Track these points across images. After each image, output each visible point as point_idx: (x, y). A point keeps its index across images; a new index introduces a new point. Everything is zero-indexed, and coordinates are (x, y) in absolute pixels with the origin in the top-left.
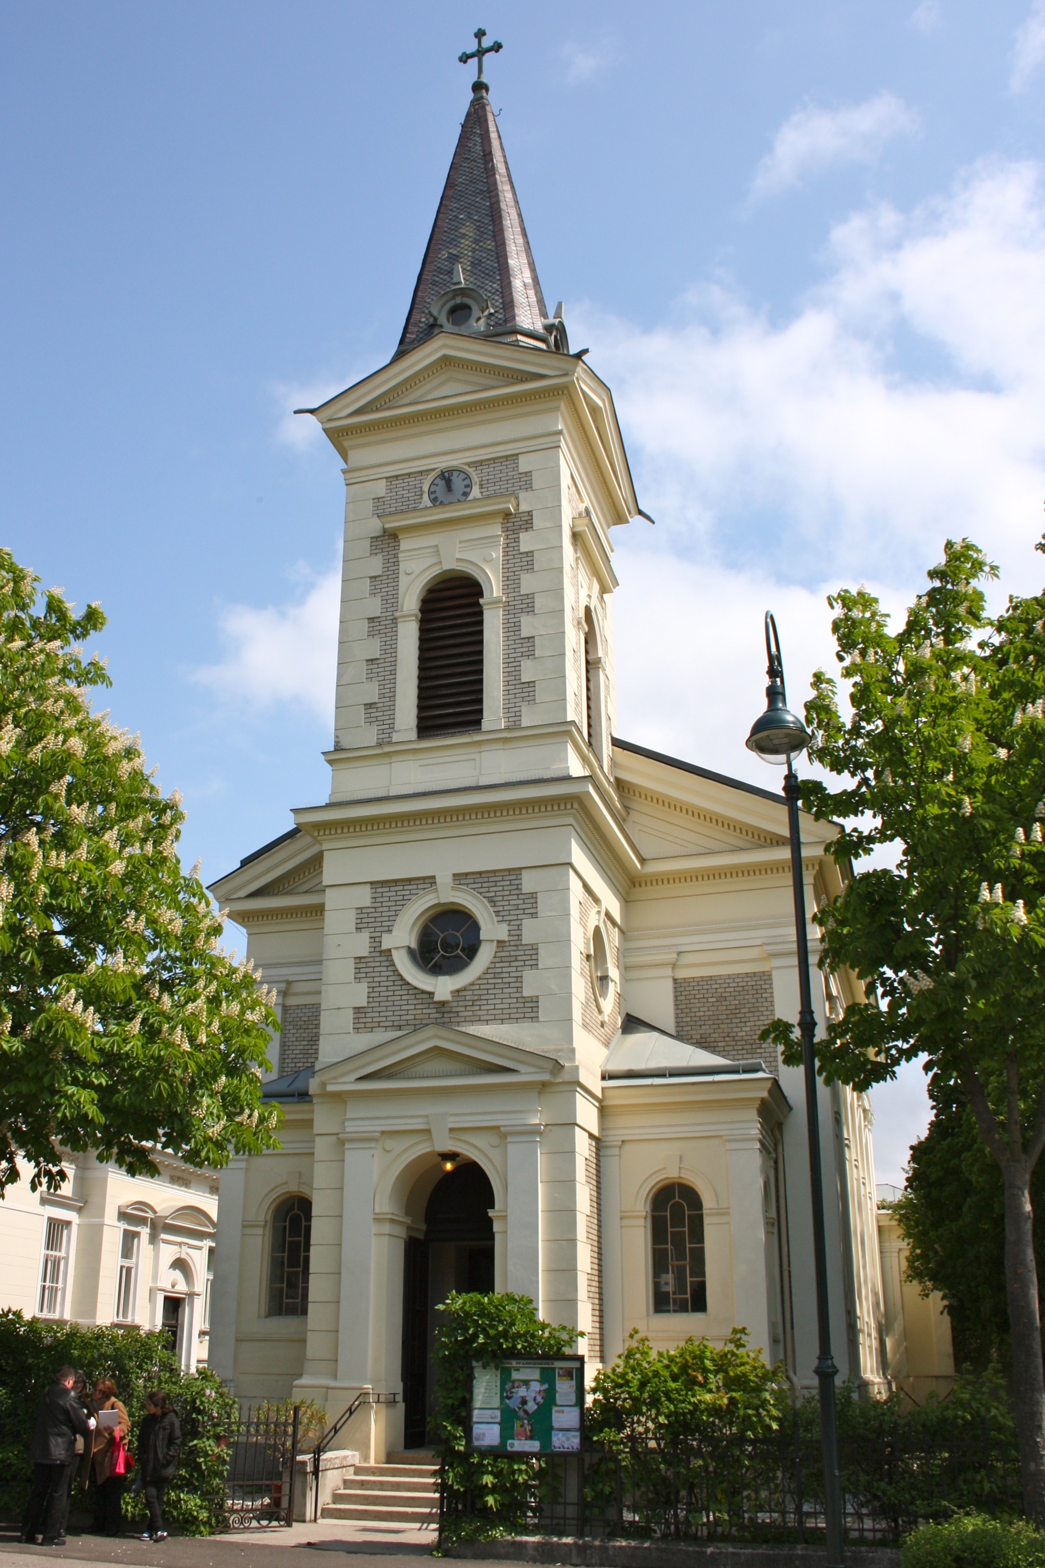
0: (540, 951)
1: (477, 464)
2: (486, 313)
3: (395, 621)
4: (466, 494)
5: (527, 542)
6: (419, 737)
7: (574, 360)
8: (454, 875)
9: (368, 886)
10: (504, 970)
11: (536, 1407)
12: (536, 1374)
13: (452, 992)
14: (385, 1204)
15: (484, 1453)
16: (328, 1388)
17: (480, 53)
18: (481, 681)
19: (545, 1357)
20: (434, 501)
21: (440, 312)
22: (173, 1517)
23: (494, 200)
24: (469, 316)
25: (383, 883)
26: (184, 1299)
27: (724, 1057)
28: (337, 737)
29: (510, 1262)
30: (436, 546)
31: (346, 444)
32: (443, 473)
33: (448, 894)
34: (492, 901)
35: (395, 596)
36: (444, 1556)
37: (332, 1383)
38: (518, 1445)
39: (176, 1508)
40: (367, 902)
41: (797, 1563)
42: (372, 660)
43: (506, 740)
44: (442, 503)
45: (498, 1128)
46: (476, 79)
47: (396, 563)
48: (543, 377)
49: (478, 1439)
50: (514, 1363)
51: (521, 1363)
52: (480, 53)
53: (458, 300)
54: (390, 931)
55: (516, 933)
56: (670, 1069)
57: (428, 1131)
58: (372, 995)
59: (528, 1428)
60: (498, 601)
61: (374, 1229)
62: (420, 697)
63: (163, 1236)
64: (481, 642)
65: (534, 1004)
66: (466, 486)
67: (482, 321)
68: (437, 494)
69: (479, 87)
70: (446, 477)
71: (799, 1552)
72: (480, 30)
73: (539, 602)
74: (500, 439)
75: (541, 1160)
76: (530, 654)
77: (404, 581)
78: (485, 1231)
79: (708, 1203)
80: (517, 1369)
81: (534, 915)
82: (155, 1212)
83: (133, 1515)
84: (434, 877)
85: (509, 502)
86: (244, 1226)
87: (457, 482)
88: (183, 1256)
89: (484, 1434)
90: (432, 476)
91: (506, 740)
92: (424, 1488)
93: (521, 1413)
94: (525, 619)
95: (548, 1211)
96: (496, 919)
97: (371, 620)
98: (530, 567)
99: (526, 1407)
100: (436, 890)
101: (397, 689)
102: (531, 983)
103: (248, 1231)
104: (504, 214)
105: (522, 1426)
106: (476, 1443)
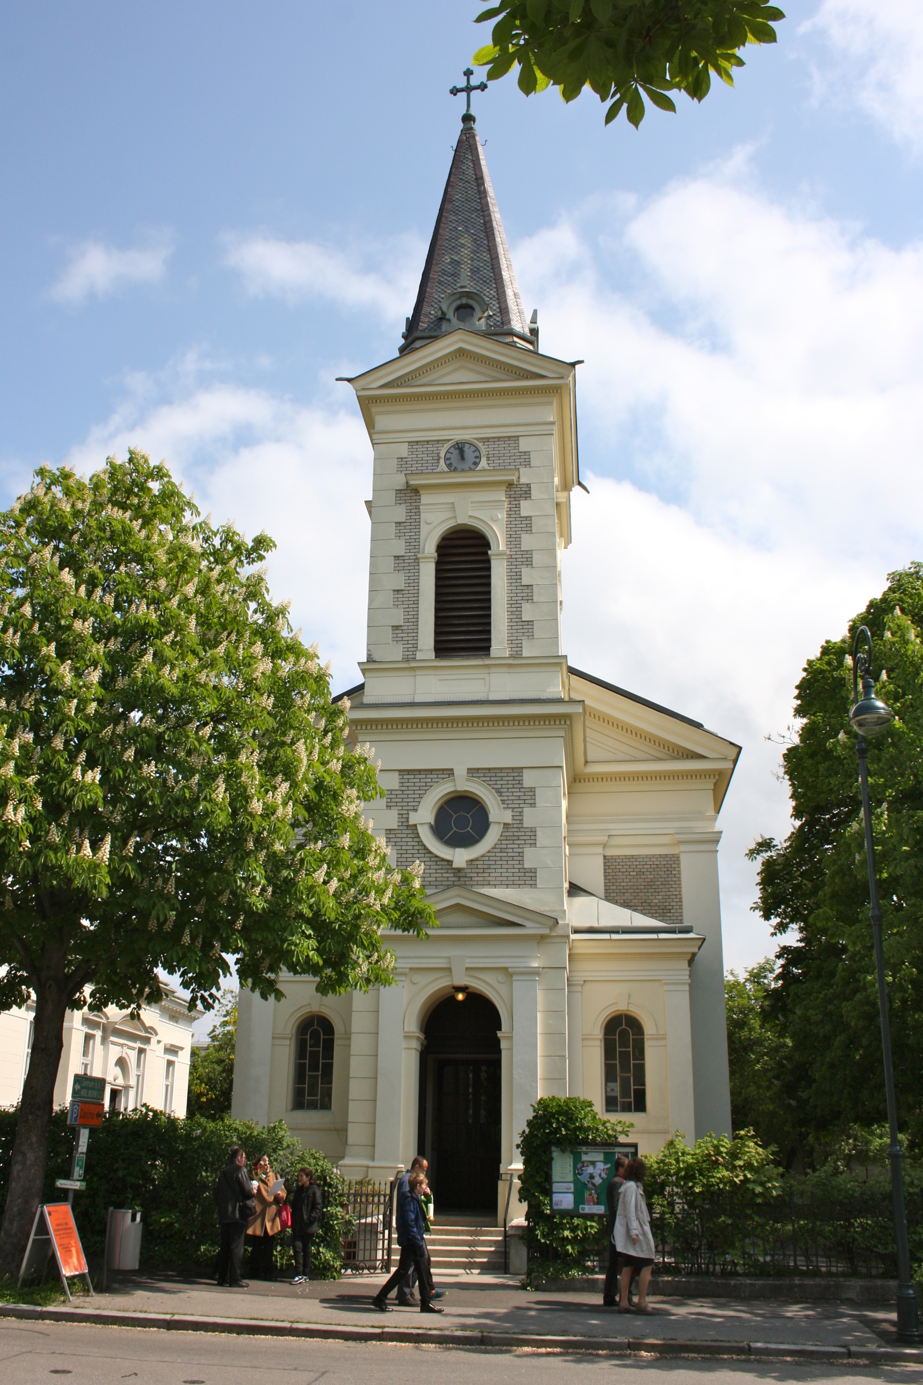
0: (538, 833)
1: (485, 440)
2: (486, 314)
3: (417, 560)
4: (476, 464)
5: (526, 508)
6: (436, 657)
7: (569, 367)
8: (468, 769)
9: (397, 773)
10: (509, 846)
11: (601, 1181)
12: (601, 1157)
13: (467, 861)
14: (412, 1025)
15: (564, 1214)
16: (368, 1167)
17: (468, 89)
18: (489, 616)
19: (605, 1144)
20: (449, 466)
21: (448, 308)
22: (315, 1265)
23: (487, 219)
24: (472, 315)
25: (409, 772)
26: (121, 1091)
27: (655, 918)
28: (369, 650)
29: (514, 1072)
30: (453, 503)
31: (374, 410)
32: (457, 444)
33: (463, 784)
34: (499, 792)
35: (417, 540)
36: (536, 1290)
37: (371, 1164)
38: (587, 1209)
39: (316, 1259)
40: (396, 786)
41: (796, 1290)
42: (398, 591)
43: (510, 665)
44: (455, 470)
45: (506, 969)
46: (465, 112)
47: (418, 513)
48: (543, 377)
49: (556, 1205)
50: (584, 1149)
51: (590, 1149)
52: (468, 89)
53: (464, 301)
54: (416, 810)
55: (519, 817)
56: (622, 927)
57: (449, 969)
58: (400, 860)
59: (595, 1196)
60: (502, 554)
61: (404, 1044)
62: (437, 625)
63: (112, 1039)
64: (489, 584)
65: (533, 875)
66: (476, 457)
67: (483, 320)
68: (452, 461)
69: (468, 119)
70: (460, 448)
71: (797, 1282)
72: (468, 69)
73: (537, 558)
74: (504, 422)
75: (540, 995)
76: (530, 599)
77: (424, 529)
78: (495, 1047)
79: (649, 1029)
80: (586, 1153)
81: (533, 805)
82: (107, 1018)
83: (282, 1264)
84: (452, 770)
85: (514, 475)
86: (273, 1038)
87: (469, 453)
88: (124, 1055)
89: (561, 1201)
90: (447, 446)
91: (510, 665)
92: (434, 1242)
93: (590, 1185)
94: (525, 571)
95: (544, 1034)
96: (502, 806)
97: (397, 557)
98: (529, 529)
99: (594, 1181)
100: (454, 780)
101: (420, 616)
102: (530, 858)
103: (277, 1042)
104: (496, 233)
105: (590, 1195)
106: (555, 1207)
